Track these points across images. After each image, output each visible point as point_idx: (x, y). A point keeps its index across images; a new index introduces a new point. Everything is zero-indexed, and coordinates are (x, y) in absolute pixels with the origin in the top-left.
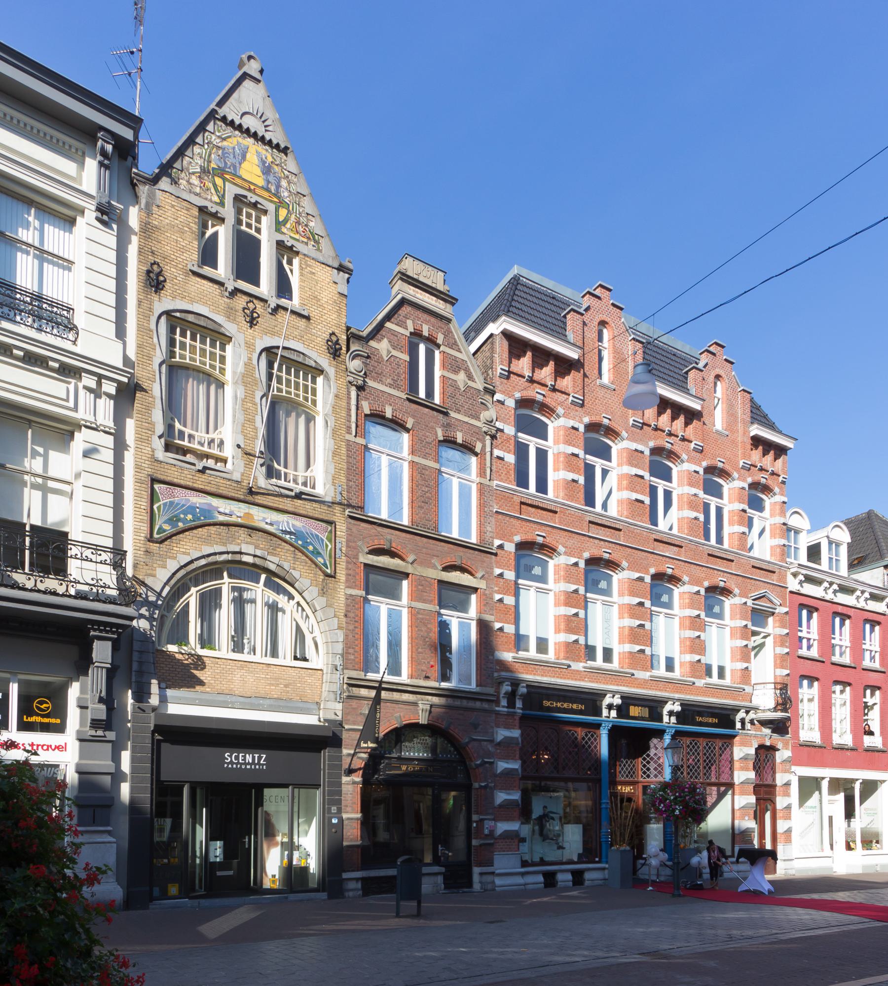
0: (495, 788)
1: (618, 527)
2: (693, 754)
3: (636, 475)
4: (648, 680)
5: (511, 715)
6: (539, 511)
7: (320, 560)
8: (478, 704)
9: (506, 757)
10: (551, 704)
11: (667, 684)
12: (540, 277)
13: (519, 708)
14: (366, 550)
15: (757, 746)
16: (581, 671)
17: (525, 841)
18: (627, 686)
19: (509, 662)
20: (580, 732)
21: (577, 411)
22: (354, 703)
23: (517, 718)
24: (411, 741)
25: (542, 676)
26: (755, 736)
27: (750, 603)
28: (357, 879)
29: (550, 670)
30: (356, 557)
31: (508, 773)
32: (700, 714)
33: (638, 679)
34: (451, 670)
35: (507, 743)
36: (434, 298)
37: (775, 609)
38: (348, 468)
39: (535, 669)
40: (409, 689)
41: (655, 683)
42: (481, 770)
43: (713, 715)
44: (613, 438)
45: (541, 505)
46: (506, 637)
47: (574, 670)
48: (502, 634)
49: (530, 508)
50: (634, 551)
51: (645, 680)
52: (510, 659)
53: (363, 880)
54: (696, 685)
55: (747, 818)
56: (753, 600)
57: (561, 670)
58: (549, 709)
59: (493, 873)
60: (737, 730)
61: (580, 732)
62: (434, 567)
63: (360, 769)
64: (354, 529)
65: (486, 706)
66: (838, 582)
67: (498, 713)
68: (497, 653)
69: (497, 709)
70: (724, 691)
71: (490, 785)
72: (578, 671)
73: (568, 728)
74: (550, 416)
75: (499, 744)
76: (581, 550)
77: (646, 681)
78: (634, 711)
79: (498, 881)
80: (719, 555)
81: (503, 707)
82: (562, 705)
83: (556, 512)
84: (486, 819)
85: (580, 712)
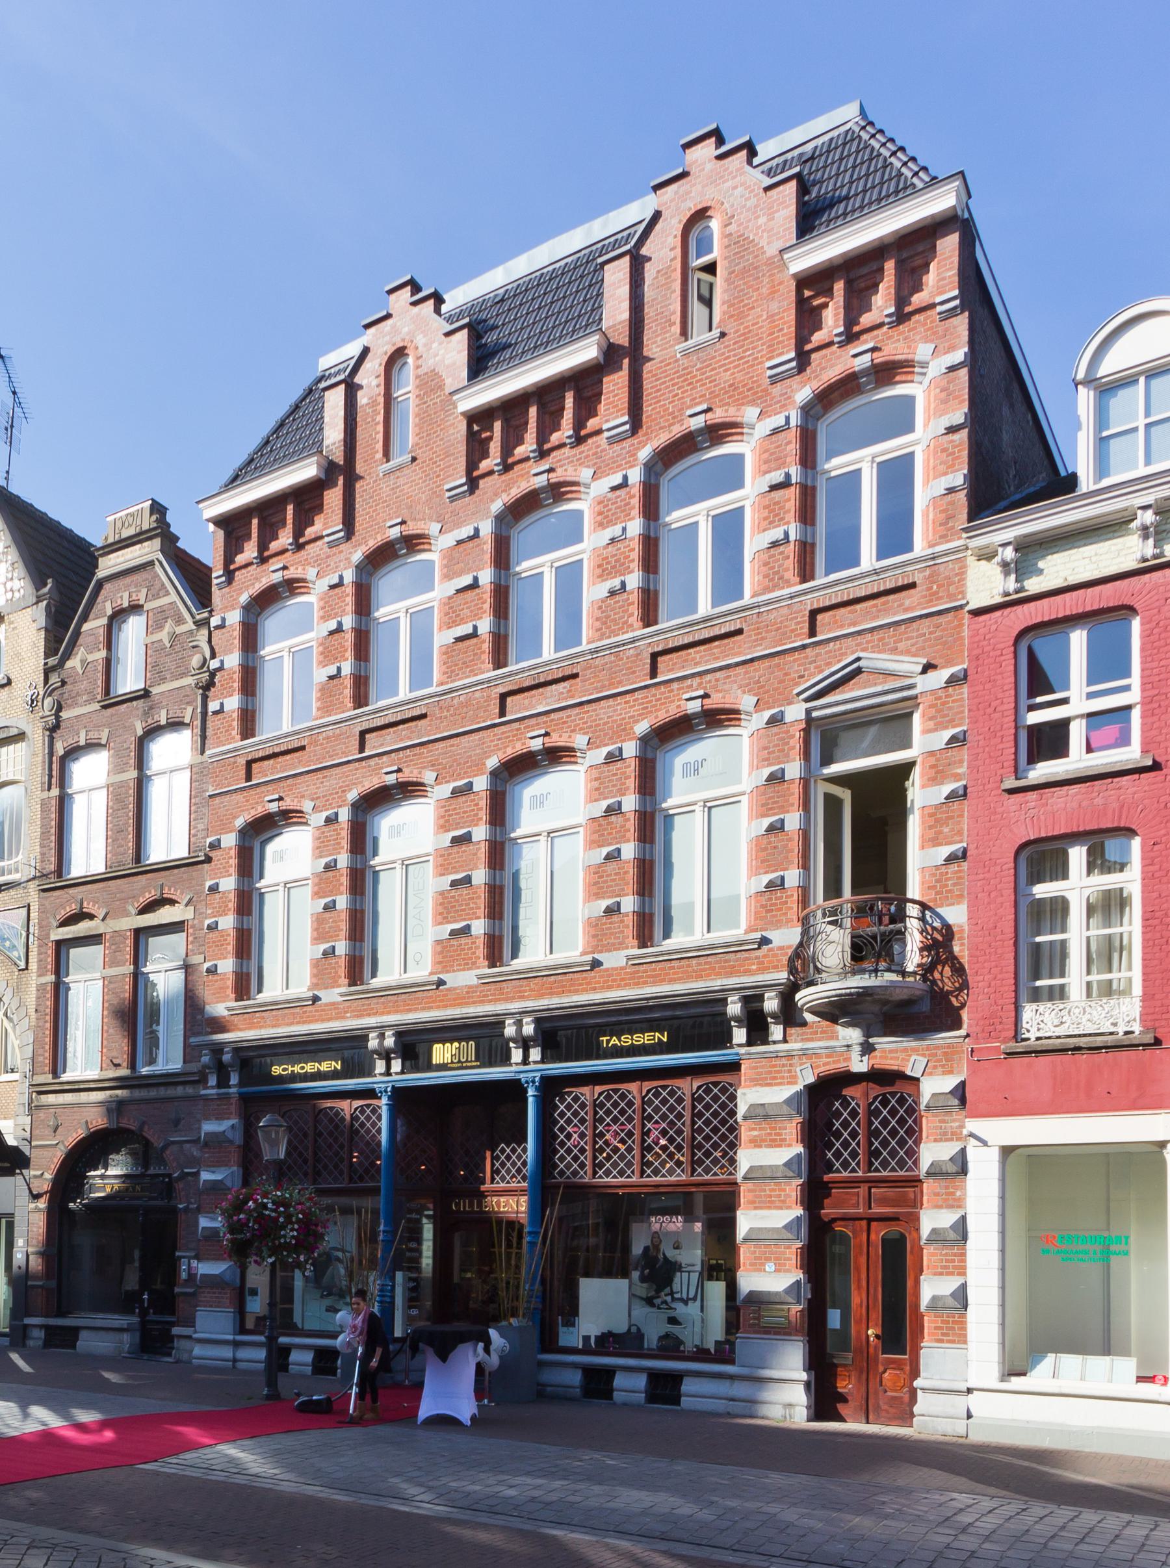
0: (199, 1210)
1: (568, 672)
2: (615, 1120)
3: (459, 591)
4: (477, 987)
5: (225, 1098)
6: (280, 759)
7: (16, 954)
8: (179, 1091)
9: (214, 1165)
10: (284, 1070)
11: (525, 982)
12: (800, 128)
13: (234, 1086)
14: (55, 924)
15: (811, 1079)
16: (338, 1003)
17: (256, 1294)
18: (438, 1007)
19: (224, 1017)
20: (347, 1107)
21: (341, 552)
22: (41, 1114)
23: (233, 1101)
24: (118, 1152)
25: (273, 1026)
26: (804, 1054)
27: (795, 712)
28: (40, 1327)
29: (284, 1016)
30: (48, 935)
31: (215, 1186)
32: (617, 1029)
33: (455, 989)
34: (158, 1048)
35: (215, 1142)
36: (138, 547)
37: (911, 687)
38: (42, 833)
39: (263, 1018)
40: (92, 1085)
41: (493, 987)
42: (181, 1185)
43: (652, 1025)
44: (426, 547)
45: (277, 750)
46: (222, 979)
47: (326, 1005)
48: (216, 977)
49: (266, 763)
50: (452, 741)
51: (470, 987)
52: (226, 1013)
53: (47, 1328)
54: (324, 1001)
55: (770, 1267)
56: (807, 700)
57: (305, 1009)
58: (281, 1079)
59: (189, 1337)
60: (736, 1050)
61: (347, 1107)
62: (128, 915)
63: (46, 1193)
64: (47, 903)
65: (190, 1090)
66: (1149, 498)
67: (205, 1099)
68: (207, 1008)
69: (203, 1092)
70: (694, 961)
71: (191, 1206)
72: (333, 1004)
73: (328, 1104)
74: (909, 377)
75: (206, 1144)
76: (344, 791)
77: (471, 989)
78: (442, 1053)
79: (198, 1350)
80: (687, 640)
81: (212, 1087)
82: (302, 1068)
83: (303, 748)
84: (184, 1257)
85: (335, 1075)
